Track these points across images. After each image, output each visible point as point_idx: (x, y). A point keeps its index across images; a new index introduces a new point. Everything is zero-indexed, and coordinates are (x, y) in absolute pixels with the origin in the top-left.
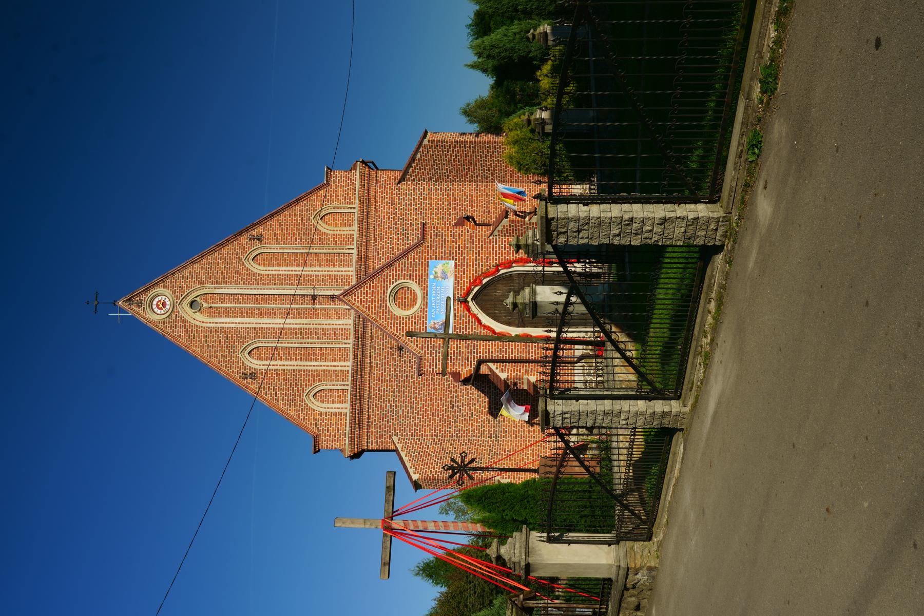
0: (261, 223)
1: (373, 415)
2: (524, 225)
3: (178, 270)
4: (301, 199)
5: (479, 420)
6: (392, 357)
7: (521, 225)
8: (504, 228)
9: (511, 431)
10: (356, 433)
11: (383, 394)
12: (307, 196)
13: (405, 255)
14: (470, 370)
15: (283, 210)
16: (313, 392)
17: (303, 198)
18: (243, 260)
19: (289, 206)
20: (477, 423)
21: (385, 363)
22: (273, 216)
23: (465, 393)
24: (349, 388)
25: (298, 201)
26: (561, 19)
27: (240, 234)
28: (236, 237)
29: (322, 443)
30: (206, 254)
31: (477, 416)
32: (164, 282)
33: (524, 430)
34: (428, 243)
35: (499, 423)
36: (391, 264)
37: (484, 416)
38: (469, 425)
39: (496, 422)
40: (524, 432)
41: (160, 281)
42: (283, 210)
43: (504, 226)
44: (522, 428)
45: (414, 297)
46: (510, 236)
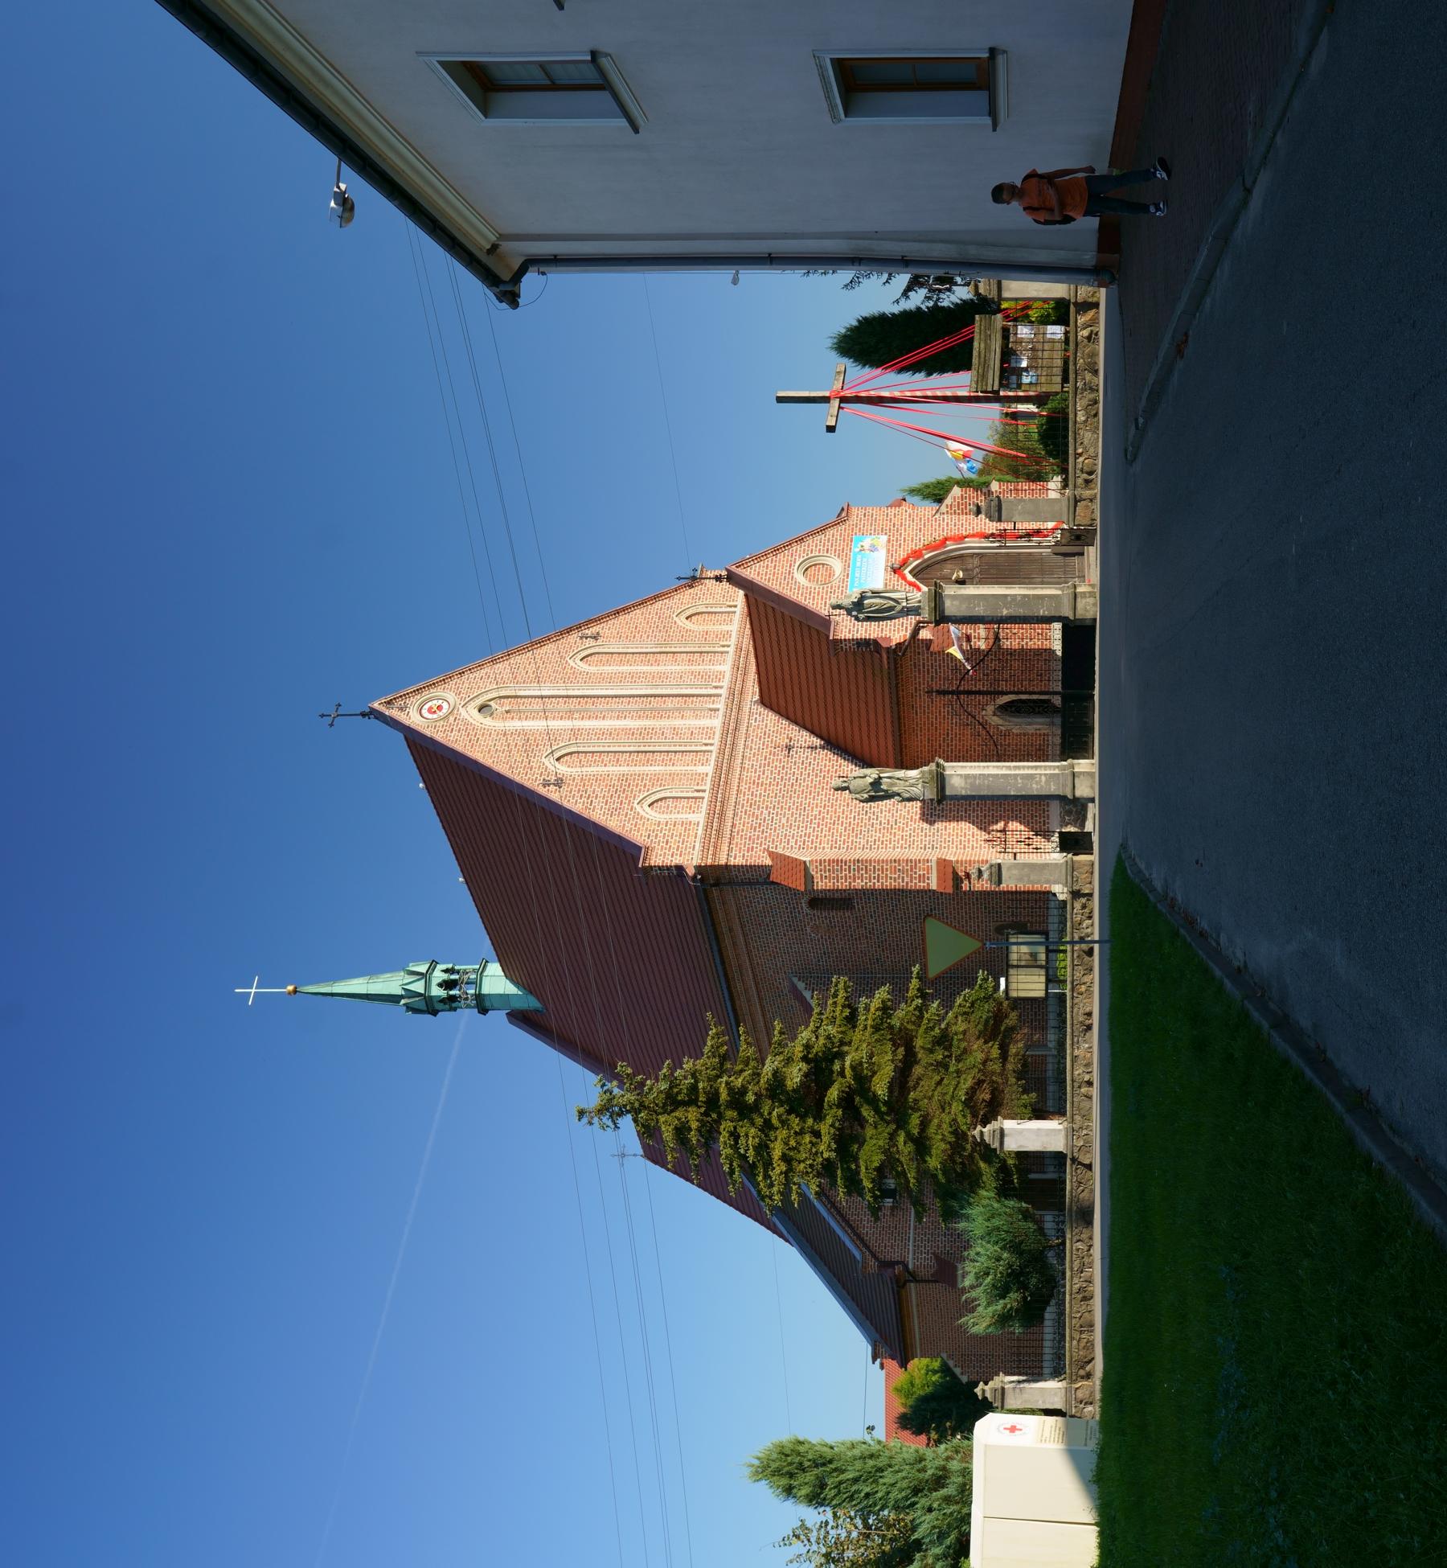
0: (600, 620)
1: (740, 823)
3: (470, 670)
4: (661, 596)
5: (905, 829)
6: (775, 758)
8: (955, 501)
11: (758, 799)
12: (670, 593)
13: (821, 531)
14: (905, 636)
15: (634, 607)
16: (650, 801)
17: (664, 595)
18: (568, 659)
19: (643, 603)
21: (765, 764)
22: (618, 613)
24: (706, 795)
25: (656, 598)
26: (1024, 456)
27: (568, 632)
28: (561, 634)
29: (656, 857)
30: (515, 653)
32: (445, 683)
34: (853, 521)
38: (891, 834)
39: (932, 831)
41: (441, 681)
42: (634, 607)
45: (830, 574)
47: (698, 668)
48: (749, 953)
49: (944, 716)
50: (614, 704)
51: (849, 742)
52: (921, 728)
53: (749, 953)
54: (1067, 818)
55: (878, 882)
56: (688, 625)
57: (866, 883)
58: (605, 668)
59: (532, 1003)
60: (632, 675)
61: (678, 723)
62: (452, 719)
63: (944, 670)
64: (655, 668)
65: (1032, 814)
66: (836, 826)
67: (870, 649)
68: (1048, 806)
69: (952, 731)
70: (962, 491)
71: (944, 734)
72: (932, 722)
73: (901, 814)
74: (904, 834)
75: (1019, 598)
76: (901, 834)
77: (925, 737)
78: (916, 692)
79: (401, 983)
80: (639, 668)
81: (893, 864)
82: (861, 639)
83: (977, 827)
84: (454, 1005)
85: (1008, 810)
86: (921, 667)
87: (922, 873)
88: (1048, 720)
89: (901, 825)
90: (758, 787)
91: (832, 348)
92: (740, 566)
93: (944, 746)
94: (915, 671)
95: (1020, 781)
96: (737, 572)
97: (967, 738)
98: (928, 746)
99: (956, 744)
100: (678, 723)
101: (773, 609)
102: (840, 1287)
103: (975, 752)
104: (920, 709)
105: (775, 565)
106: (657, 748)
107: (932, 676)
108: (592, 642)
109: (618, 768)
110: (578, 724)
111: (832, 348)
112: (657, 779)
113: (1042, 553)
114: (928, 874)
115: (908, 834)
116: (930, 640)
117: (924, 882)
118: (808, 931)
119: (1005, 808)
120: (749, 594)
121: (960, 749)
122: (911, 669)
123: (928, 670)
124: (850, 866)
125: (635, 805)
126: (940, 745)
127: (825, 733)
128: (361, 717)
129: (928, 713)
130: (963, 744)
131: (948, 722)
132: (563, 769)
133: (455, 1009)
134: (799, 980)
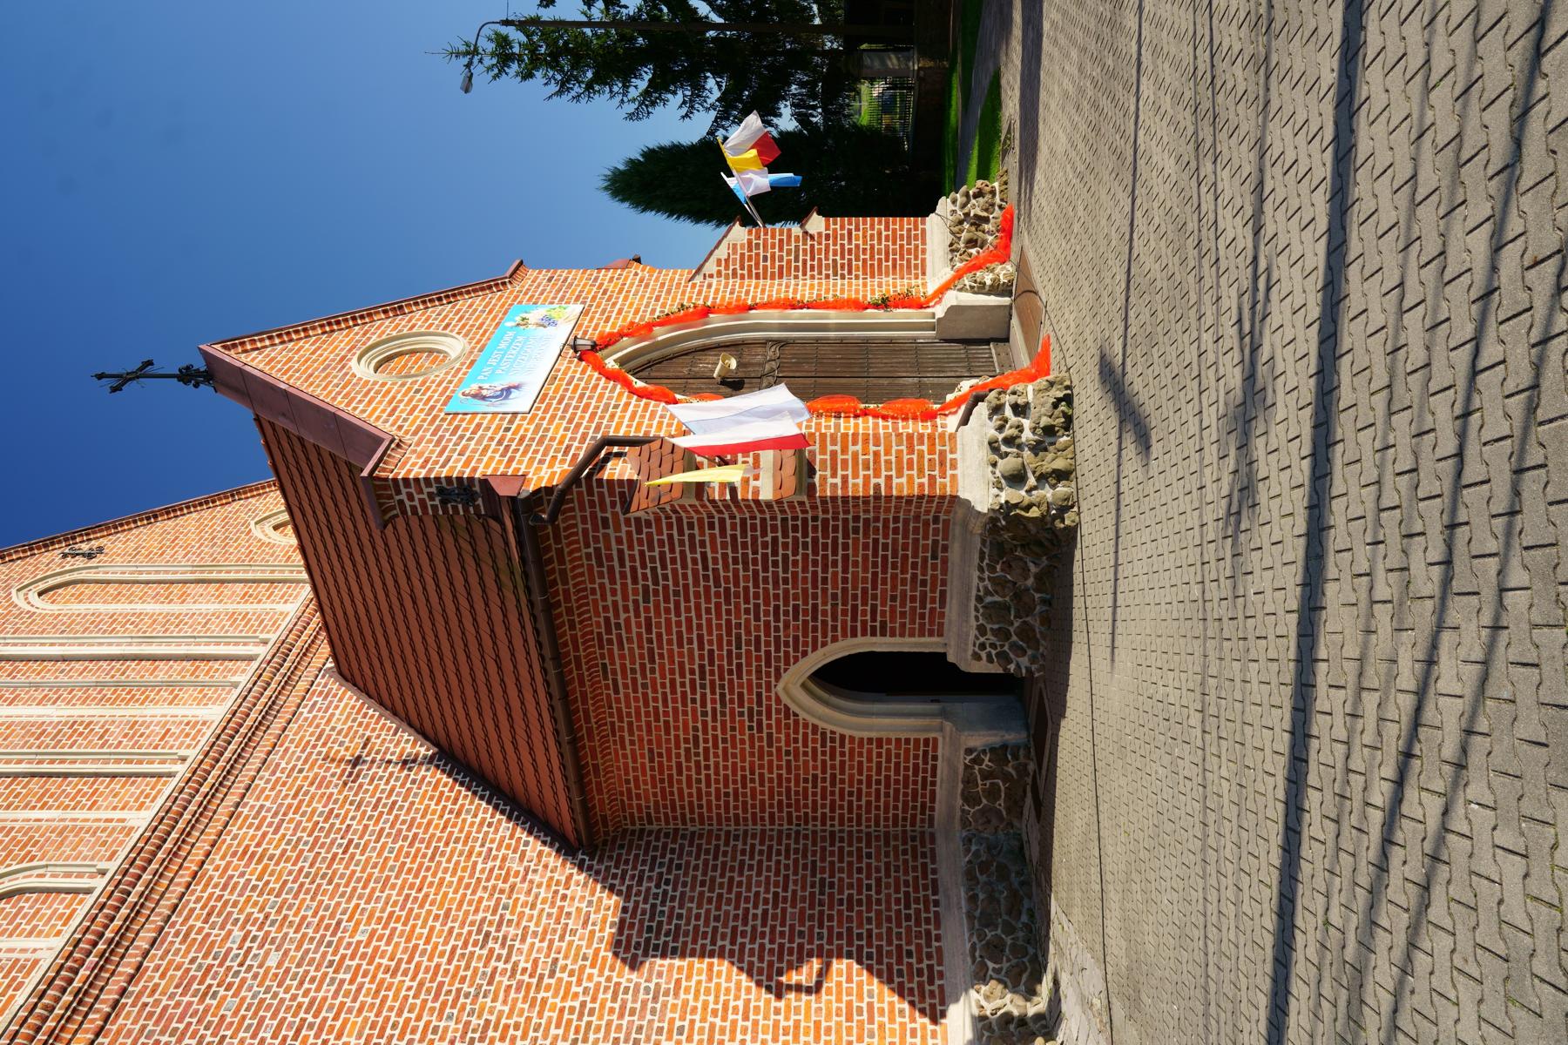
2: (789, 243)
5: (574, 989)
7: (781, 241)
8: (735, 252)
9: (701, 1030)
10: (50, 1024)
20: (564, 999)
22: (155, 517)
23: (542, 895)
31: (571, 974)
33: (756, 1023)
35: (655, 999)
36: (401, 308)
37: (601, 974)
38: (532, 1005)
40: (755, 1031)
43: (735, 246)
44: (746, 1018)
46: (750, 277)
49: (684, 694)
50: (51, 675)
51: (471, 754)
52: (630, 724)
54: (991, 965)
63: (675, 571)
64: (175, 608)
65: (899, 947)
67: (477, 508)
68: (938, 926)
69: (705, 732)
70: (750, 233)
71: (687, 741)
72: (656, 709)
73: (571, 943)
74: (568, 1004)
76: (560, 1005)
77: (641, 748)
78: (609, 632)
82: (449, 479)
83: (759, 984)
85: (840, 936)
86: (616, 563)
88: (935, 707)
89: (565, 976)
91: (606, 188)
92: (234, 346)
93: (689, 769)
94: (601, 575)
96: (228, 359)
97: (743, 750)
98: (652, 769)
99: (717, 764)
101: (286, 432)
103: (762, 785)
104: (624, 676)
106: (77, 768)
107: (646, 588)
111: (606, 188)
113: (915, 339)
115: (577, 1004)
116: (630, 481)
119: (830, 929)
120: (264, 416)
121: (726, 777)
122: (590, 568)
126: (679, 765)
127: (443, 741)
129: (644, 686)
130: (734, 764)
131: (694, 710)
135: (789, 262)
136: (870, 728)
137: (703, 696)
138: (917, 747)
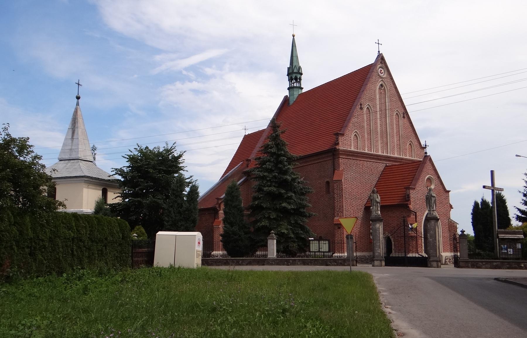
8: (453, 224)
47: (396, 147)
48: (312, 164)
53: (312, 164)
55: (336, 202)
56: (408, 144)
57: (336, 198)
58: (395, 120)
59: (291, 102)
60: (393, 128)
61: (380, 142)
62: (378, 77)
64: (395, 135)
66: (351, 189)
75: (435, 244)
79: (296, 65)
80: (395, 130)
81: (342, 206)
84: (290, 81)
87: (339, 214)
88: (385, 252)
90: (362, 166)
95: (378, 244)
100: (380, 142)
102: (211, 192)
105: (431, 170)
108: (402, 116)
109: (366, 125)
110: (378, 113)
112: (363, 137)
114: (339, 216)
117: (337, 215)
118: (319, 181)
123: (401, 216)
124: (341, 193)
125: (356, 130)
128: (378, 51)
132: (365, 109)
133: (289, 81)
134: (304, 179)
135: (451, 232)
136: (441, 245)
137: (386, 223)
138: (421, 227)
